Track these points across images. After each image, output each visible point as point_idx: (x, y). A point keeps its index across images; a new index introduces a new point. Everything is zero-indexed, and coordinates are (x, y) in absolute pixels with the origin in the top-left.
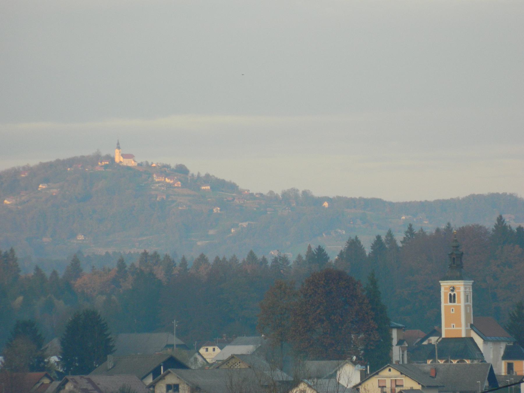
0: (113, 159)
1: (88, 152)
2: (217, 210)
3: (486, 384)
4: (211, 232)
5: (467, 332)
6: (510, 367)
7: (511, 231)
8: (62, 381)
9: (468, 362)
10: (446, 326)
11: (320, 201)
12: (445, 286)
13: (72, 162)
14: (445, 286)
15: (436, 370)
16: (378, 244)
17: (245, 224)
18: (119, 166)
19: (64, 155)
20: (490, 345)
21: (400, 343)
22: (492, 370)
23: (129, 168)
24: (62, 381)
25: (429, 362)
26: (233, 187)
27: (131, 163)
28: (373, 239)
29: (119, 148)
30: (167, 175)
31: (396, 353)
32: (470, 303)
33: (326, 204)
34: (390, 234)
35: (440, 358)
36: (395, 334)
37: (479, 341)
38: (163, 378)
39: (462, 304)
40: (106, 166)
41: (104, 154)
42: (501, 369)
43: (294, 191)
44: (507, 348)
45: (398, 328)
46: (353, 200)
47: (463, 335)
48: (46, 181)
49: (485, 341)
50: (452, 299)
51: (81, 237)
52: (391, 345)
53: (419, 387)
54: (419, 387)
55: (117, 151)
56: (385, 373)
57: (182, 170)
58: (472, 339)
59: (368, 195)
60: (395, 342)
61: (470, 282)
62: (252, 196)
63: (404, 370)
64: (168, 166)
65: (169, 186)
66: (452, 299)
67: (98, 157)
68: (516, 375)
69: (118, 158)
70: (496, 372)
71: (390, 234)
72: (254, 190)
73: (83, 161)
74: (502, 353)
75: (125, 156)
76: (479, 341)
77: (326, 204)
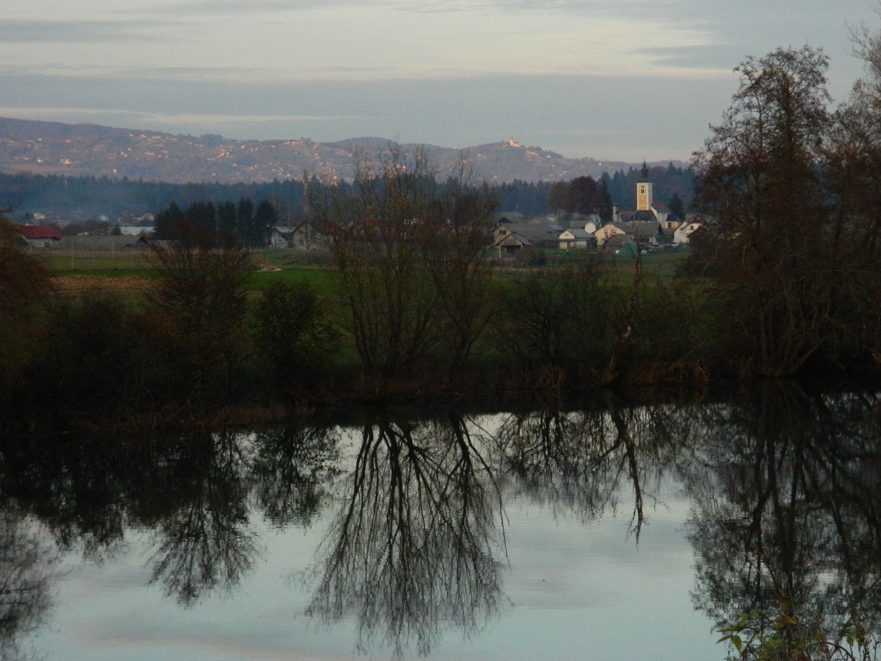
0: (509, 144)
1: (498, 140)
2: (553, 166)
3: (657, 232)
4: (551, 175)
5: (649, 207)
6: (670, 225)
7: (676, 169)
8: (72, 163)
9: (649, 222)
10: (640, 204)
11: (597, 163)
12: (639, 186)
13: (492, 145)
14: (639, 186)
15: (633, 226)
16: (616, 175)
17: (565, 172)
18: (512, 147)
19: (489, 142)
20: (660, 214)
21: (617, 213)
22: (660, 225)
23: (517, 148)
24: (72, 163)
25: (631, 222)
26: (560, 156)
27: (517, 146)
28: (614, 173)
29: (512, 139)
30: (532, 151)
31: (615, 217)
32: (651, 194)
33: (600, 164)
34: (622, 171)
35: (636, 220)
36: (614, 209)
37: (655, 212)
38: (498, 227)
39: (647, 195)
40: (506, 147)
41: (505, 141)
42: (665, 225)
43: (587, 158)
44: (668, 215)
45: (616, 206)
46: (612, 163)
47: (648, 209)
48: (481, 153)
49: (658, 212)
50: (643, 191)
51: (495, 177)
52: (612, 214)
53: (624, 233)
54: (624, 233)
55: (511, 141)
56: (608, 226)
57: (539, 149)
58: (651, 211)
59: (618, 160)
60: (614, 212)
61: (652, 184)
62: (569, 160)
63: (617, 225)
64: (533, 147)
65: (533, 156)
66: (643, 191)
67: (503, 143)
68: (848, 394)
69: (512, 144)
70: (662, 226)
71: (622, 171)
72: (570, 157)
73: (496, 144)
74: (666, 218)
75: (514, 143)
76: (655, 212)
77: (600, 164)
